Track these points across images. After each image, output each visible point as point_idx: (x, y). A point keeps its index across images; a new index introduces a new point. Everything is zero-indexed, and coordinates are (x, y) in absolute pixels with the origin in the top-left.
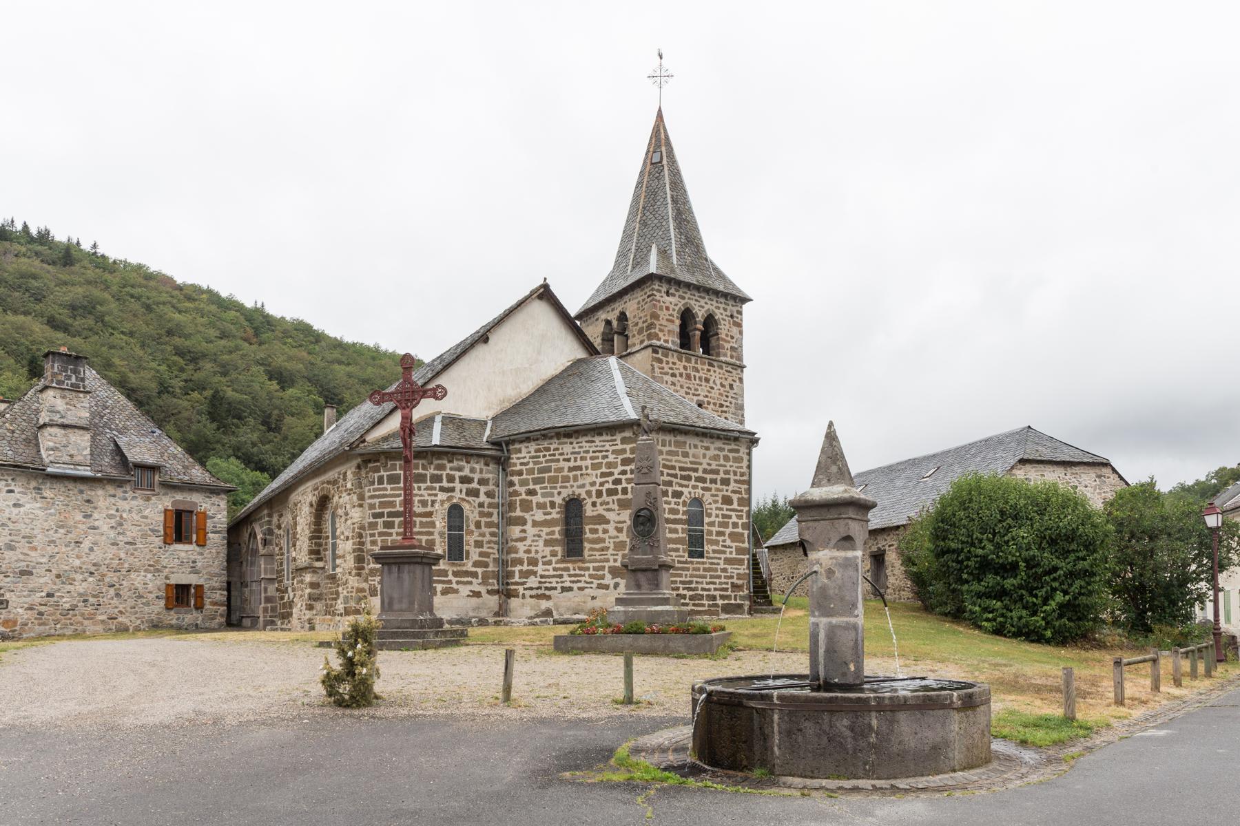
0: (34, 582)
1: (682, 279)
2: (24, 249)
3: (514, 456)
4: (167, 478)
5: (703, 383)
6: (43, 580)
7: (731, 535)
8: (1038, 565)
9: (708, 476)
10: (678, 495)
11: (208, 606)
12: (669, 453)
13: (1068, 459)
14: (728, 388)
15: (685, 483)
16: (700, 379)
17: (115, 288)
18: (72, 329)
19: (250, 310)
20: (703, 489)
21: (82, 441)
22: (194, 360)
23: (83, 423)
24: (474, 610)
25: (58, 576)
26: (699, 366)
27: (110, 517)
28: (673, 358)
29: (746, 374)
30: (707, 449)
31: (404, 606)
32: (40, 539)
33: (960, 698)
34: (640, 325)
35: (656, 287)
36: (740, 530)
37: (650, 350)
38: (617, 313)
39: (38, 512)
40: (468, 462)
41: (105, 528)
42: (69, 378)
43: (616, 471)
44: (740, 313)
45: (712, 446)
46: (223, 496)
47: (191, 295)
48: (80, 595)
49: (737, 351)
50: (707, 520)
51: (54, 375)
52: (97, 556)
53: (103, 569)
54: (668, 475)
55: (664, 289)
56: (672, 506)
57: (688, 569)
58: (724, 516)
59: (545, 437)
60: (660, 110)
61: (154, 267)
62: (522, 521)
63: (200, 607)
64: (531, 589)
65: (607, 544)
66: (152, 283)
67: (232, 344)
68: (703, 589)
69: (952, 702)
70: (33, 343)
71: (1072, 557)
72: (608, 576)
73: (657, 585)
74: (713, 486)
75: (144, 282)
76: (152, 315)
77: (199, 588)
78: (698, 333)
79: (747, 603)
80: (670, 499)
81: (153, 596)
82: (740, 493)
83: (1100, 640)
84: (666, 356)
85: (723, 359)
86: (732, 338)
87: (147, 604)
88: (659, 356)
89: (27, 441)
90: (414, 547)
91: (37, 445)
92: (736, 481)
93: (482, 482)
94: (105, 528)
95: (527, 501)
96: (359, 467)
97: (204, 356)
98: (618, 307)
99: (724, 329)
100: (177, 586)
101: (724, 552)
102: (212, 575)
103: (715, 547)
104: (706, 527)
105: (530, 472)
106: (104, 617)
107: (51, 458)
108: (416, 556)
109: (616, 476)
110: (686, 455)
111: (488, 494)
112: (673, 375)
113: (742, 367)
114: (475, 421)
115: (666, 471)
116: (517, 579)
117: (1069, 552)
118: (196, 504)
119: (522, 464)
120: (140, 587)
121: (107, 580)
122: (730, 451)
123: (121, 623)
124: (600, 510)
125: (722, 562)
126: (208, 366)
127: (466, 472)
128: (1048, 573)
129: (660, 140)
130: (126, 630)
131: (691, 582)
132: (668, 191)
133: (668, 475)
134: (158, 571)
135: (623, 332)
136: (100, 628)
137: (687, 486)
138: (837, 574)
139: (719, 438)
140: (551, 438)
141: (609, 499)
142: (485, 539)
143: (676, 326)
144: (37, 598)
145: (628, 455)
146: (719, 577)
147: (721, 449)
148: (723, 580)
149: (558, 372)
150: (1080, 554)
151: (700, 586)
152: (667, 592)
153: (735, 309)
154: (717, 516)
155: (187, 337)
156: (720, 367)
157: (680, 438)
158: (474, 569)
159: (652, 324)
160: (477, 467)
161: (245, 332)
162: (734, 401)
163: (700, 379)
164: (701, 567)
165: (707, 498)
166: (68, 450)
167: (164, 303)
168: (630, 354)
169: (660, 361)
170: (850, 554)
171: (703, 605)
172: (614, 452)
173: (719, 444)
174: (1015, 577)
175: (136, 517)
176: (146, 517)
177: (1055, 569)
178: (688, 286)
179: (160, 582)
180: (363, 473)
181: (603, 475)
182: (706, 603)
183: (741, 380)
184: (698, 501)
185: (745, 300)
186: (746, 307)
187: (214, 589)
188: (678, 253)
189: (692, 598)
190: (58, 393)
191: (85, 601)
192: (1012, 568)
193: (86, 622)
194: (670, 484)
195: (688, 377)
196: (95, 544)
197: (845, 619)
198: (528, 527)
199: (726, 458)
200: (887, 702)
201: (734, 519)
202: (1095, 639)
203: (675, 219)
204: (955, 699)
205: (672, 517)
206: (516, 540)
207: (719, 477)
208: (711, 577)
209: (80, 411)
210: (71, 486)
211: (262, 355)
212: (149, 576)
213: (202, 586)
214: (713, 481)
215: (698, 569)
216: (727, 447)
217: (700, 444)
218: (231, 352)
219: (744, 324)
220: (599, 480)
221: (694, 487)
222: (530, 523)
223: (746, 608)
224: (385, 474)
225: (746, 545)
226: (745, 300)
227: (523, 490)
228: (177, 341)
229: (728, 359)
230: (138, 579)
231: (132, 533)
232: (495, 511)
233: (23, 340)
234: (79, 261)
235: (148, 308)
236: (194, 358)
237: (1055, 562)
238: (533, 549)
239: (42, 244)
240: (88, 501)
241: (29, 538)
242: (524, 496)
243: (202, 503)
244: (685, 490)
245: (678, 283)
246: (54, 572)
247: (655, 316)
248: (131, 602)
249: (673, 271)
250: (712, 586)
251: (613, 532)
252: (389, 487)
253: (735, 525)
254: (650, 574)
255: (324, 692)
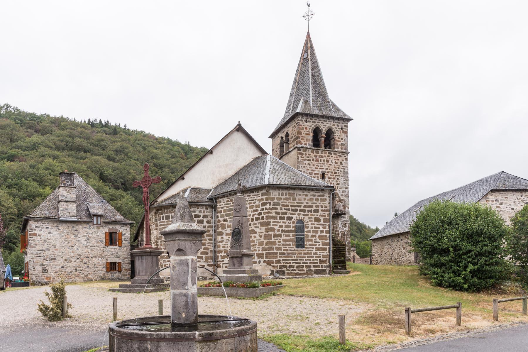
0: (57, 262)
1: (313, 113)
2: (99, 130)
3: (218, 204)
4: (106, 220)
5: (326, 163)
6: (60, 262)
7: (319, 237)
8: (460, 249)
9: (307, 209)
10: (290, 218)
11: (123, 271)
12: (285, 199)
13: (523, 187)
14: (339, 164)
15: (294, 213)
16: (324, 161)
17: (132, 142)
18: (116, 160)
19: (184, 145)
20: (303, 215)
21: (73, 207)
22: (161, 168)
23: (74, 199)
24: (201, 273)
25: (66, 260)
26: (323, 155)
27: (84, 236)
28: (309, 152)
29: (350, 157)
30: (306, 195)
31: (144, 274)
32: (58, 246)
33: (200, 335)
34: (293, 138)
35: (300, 119)
36: (324, 234)
37: (297, 149)
38: (285, 133)
39: (57, 235)
40: (198, 208)
41: (82, 241)
42: (68, 182)
43: (259, 209)
44: (347, 126)
45: (309, 194)
46: (128, 226)
47: (161, 141)
48: (74, 267)
49: (345, 146)
50: (306, 230)
51: (63, 181)
52: (80, 252)
53: (82, 257)
54: (285, 209)
55: (304, 119)
56: (287, 224)
57: (295, 254)
58: (315, 228)
59: (230, 195)
60: (308, 32)
61: (147, 131)
62: (221, 234)
63: (120, 271)
64: (226, 264)
65: (255, 243)
66: (146, 138)
67: (176, 160)
68: (303, 263)
69: (194, 337)
70: (101, 166)
71: (480, 244)
72: (256, 258)
73: (241, 264)
74: (310, 213)
75: (143, 138)
76: (146, 151)
77: (120, 263)
78: (323, 139)
79: (328, 269)
80: (286, 221)
81: (102, 267)
82: (325, 216)
83: (503, 289)
84: (305, 151)
85: (336, 150)
86: (342, 139)
87: (99, 270)
88: (302, 152)
89: (54, 208)
90: (159, 249)
91: (58, 209)
92: (322, 210)
93: (205, 217)
94: (82, 241)
95: (223, 224)
96: (155, 213)
97: (165, 166)
98: (285, 130)
99: (337, 135)
100: (111, 263)
101: (316, 245)
102: (124, 258)
103: (310, 243)
104: (305, 233)
105: (225, 211)
106: (83, 276)
107: (62, 214)
108: (147, 252)
109: (259, 211)
110: (294, 199)
111: (208, 222)
112: (309, 160)
113: (347, 153)
114: (206, 189)
115: (283, 208)
116: (220, 259)
117: (479, 242)
118: (117, 230)
119: (221, 208)
120: (97, 263)
121: (84, 261)
122: (319, 196)
123: (89, 278)
124: (253, 227)
125: (314, 250)
126: (166, 170)
127: (197, 213)
128: (464, 254)
129: (308, 47)
130: (92, 280)
131: (297, 260)
132: (310, 71)
133: (285, 209)
134: (103, 257)
135: (287, 142)
136: (81, 280)
137: (295, 214)
138: (177, 269)
139: (313, 190)
140: (233, 195)
141: (256, 222)
142: (206, 242)
143: (311, 137)
144: (58, 268)
145: (264, 201)
146: (313, 257)
147: (314, 195)
148: (315, 258)
149: (247, 164)
150: (485, 243)
151: (302, 262)
152: (246, 268)
153: (343, 125)
154: (312, 228)
155: (158, 159)
156: (335, 154)
157: (291, 191)
158: (201, 255)
159: (298, 137)
160: (202, 210)
161: (181, 154)
162: (342, 170)
163: (324, 161)
164: (303, 252)
165: (306, 219)
166: (68, 211)
167: (150, 146)
168: (289, 152)
169: (302, 154)
170: (183, 258)
171: (304, 270)
172: (259, 200)
173: (313, 193)
174: (448, 256)
175: (94, 236)
176: (98, 236)
177: (470, 251)
178: (317, 116)
179: (104, 261)
180: (157, 215)
181: (254, 211)
182: (306, 269)
183: (347, 159)
184: (301, 221)
185: (349, 120)
186: (350, 124)
187: (125, 264)
188: (313, 101)
189: (297, 267)
190: (64, 189)
191: (76, 269)
192: (445, 252)
193: (76, 278)
194: (286, 213)
195: (317, 160)
196: (79, 247)
197: (180, 291)
198: (224, 236)
199: (317, 200)
200: (155, 336)
201: (321, 229)
202: (500, 289)
203: (313, 85)
204: (197, 336)
205: (287, 229)
206: (220, 242)
207: (313, 209)
208: (308, 257)
209: (72, 195)
210: (69, 224)
211: (188, 164)
212: (100, 259)
213: (120, 263)
214: (309, 211)
215: (301, 254)
216: (317, 194)
217: (302, 194)
218: (175, 164)
219: (349, 132)
220: (252, 214)
221: (299, 214)
222: (225, 234)
223: (328, 272)
224: (164, 215)
225: (328, 241)
226: (349, 120)
227: (222, 219)
228: (155, 161)
229: (340, 150)
230: (95, 260)
231: (93, 242)
232: (211, 229)
233: (98, 166)
234: (119, 132)
235: (144, 148)
236: (160, 167)
237: (469, 247)
238: (226, 246)
239: (106, 127)
240: (76, 230)
241: (54, 246)
242: (222, 222)
243: (120, 229)
244: (294, 216)
245: (312, 116)
246: (64, 258)
247: (300, 133)
248: (93, 270)
249: (309, 110)
250: (309, 262)
251: (258, 238)
252: (166, 221)
253: (322, 232)
254: (239, 259)
255: (41, 314)
